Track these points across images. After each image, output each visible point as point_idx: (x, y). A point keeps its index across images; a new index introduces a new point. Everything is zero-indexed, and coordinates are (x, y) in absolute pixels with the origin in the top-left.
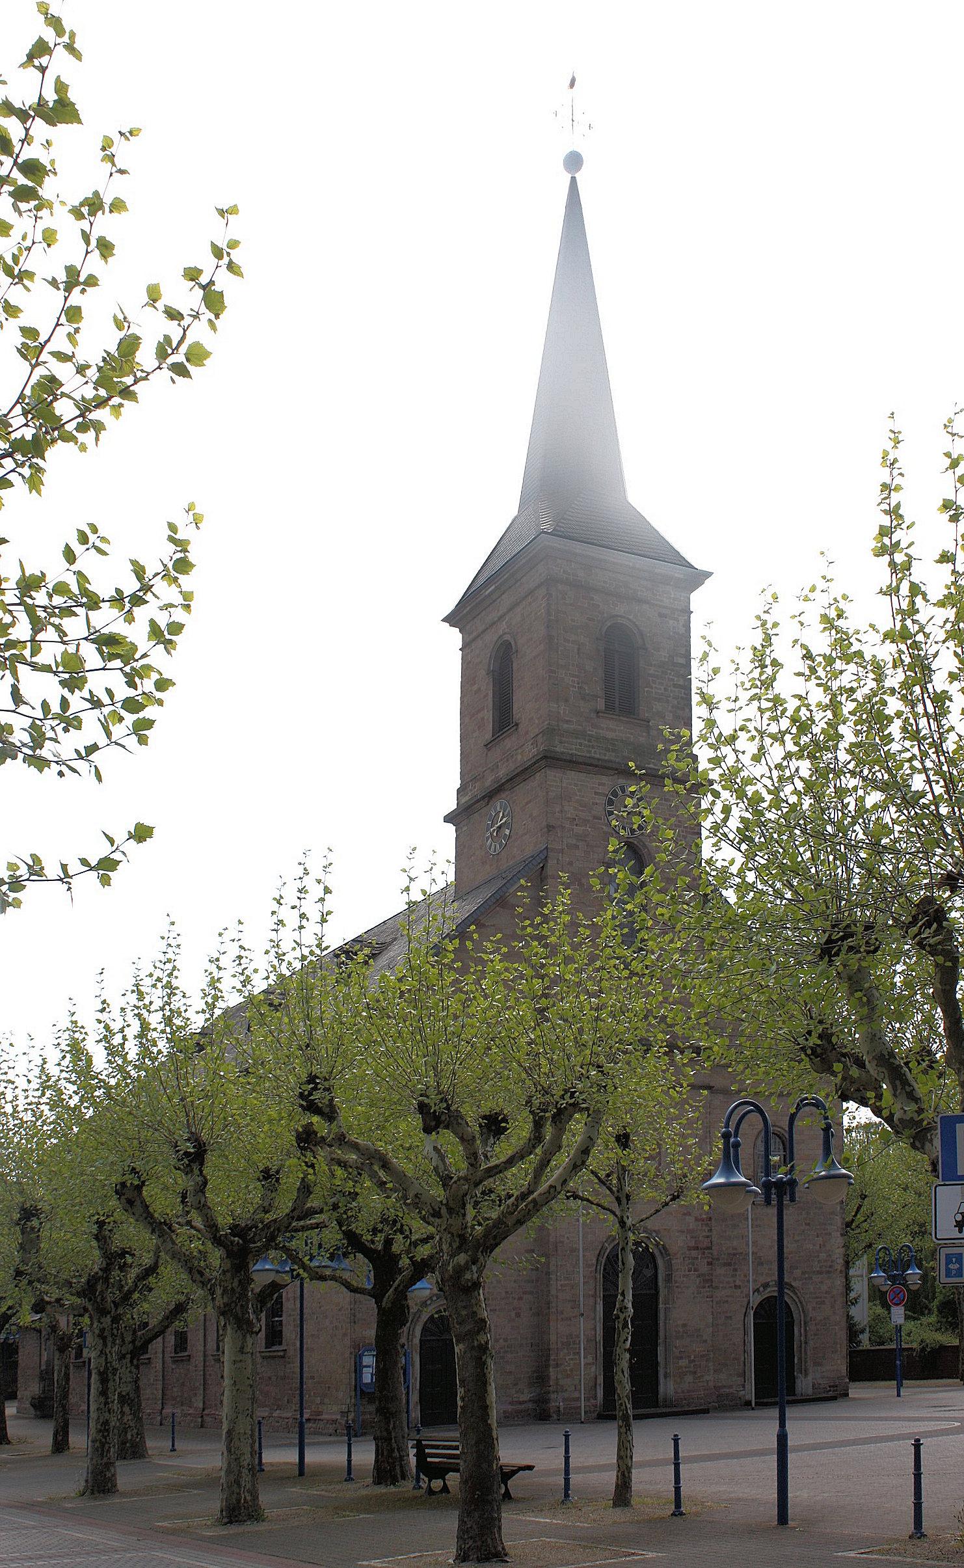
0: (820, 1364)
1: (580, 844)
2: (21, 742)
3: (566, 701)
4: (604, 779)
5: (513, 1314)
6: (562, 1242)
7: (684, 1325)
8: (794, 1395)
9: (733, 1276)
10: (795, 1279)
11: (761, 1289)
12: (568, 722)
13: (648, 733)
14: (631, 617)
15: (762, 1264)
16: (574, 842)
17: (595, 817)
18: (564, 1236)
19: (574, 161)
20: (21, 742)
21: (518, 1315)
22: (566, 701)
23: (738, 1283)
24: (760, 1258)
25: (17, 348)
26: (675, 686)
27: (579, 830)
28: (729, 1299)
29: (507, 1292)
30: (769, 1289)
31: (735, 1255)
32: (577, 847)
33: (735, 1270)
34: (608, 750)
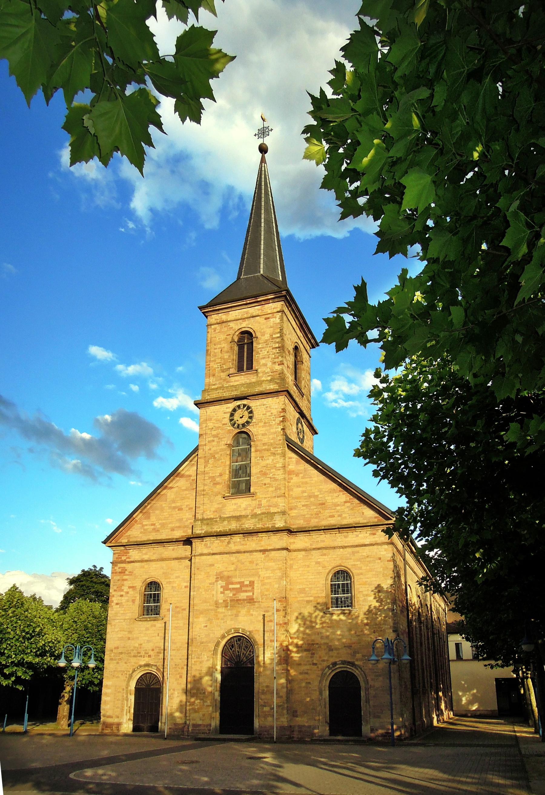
0: (379, 717)
1: (215, 439)
2: (334, 312)
3: (214, 375)
4: (229, 405)
5: (178, 676)
6: (196, 638)
7: (267, 686)
8: (361, 736)
9: (311, 657)
10: (357, 660)
11: (331, 666)
12: (214, 385)
13: (257, 375)
14: (250, 326)
15: (332, 650)
16: (212, 439)
17: (224, 424)
18: (197, 635)
19: (263, 149)
20: (334, 312)
21: (181, 677)
22: (214, 375)
23: (315, 662)
24: (331, 646)
25: (312, 97)
26: (273, 349)
27: (214, 433)
28: (309, 672)
29: (176, 665)
30: (337, 666)
31: (313, 644)
32: (213, 441)
33: (313, 654)
34: (232, 391)
